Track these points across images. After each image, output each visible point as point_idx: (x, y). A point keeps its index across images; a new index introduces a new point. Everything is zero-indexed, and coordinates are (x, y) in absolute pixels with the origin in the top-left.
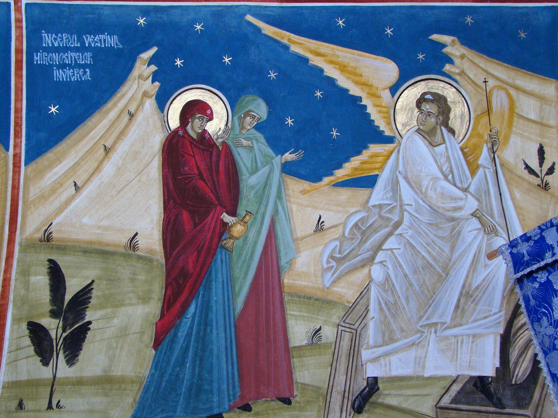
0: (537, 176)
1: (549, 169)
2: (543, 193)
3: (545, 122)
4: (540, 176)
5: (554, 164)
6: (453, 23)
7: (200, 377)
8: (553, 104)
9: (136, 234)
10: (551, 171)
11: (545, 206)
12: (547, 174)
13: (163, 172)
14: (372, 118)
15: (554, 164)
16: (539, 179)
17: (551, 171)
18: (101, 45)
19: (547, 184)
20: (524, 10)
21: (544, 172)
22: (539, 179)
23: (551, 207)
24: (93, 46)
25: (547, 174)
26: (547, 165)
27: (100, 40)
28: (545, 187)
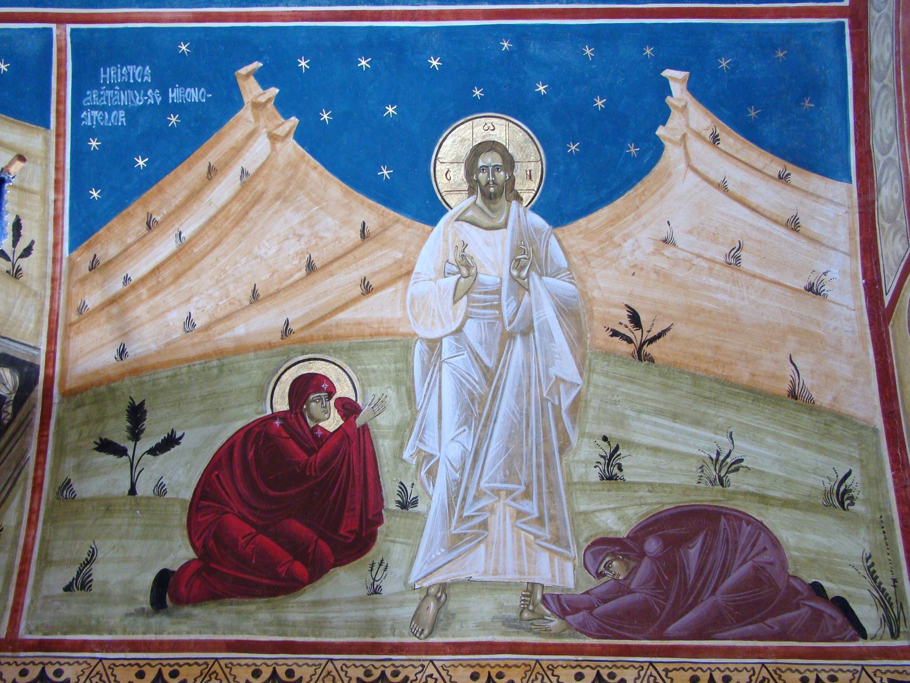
0: (8, 259)
1: (25, 250)
2: (11, 282)
3: (26, 185)
4: (11, 258)
5: (33, 242)
6: (689, 49)
7: (373, 348)
8: (39, 161)
9: (364, 223)
10: (27, 252)
11: (10, 300)
12: (22, 256)
13: (766, 150)
14: (660, 131)
15: (33, 242)
16: (10, 263)
17: (27, 252)
18: (129, 79)
19: (19, 270)
20: (7, 34)
21: (18, 254)
22: (10, 263)
23: (19, 301)
24: (140, 80)
25: (22, 256)
26: (22, 245)
27: (129, 74)
28: (16, 273)
